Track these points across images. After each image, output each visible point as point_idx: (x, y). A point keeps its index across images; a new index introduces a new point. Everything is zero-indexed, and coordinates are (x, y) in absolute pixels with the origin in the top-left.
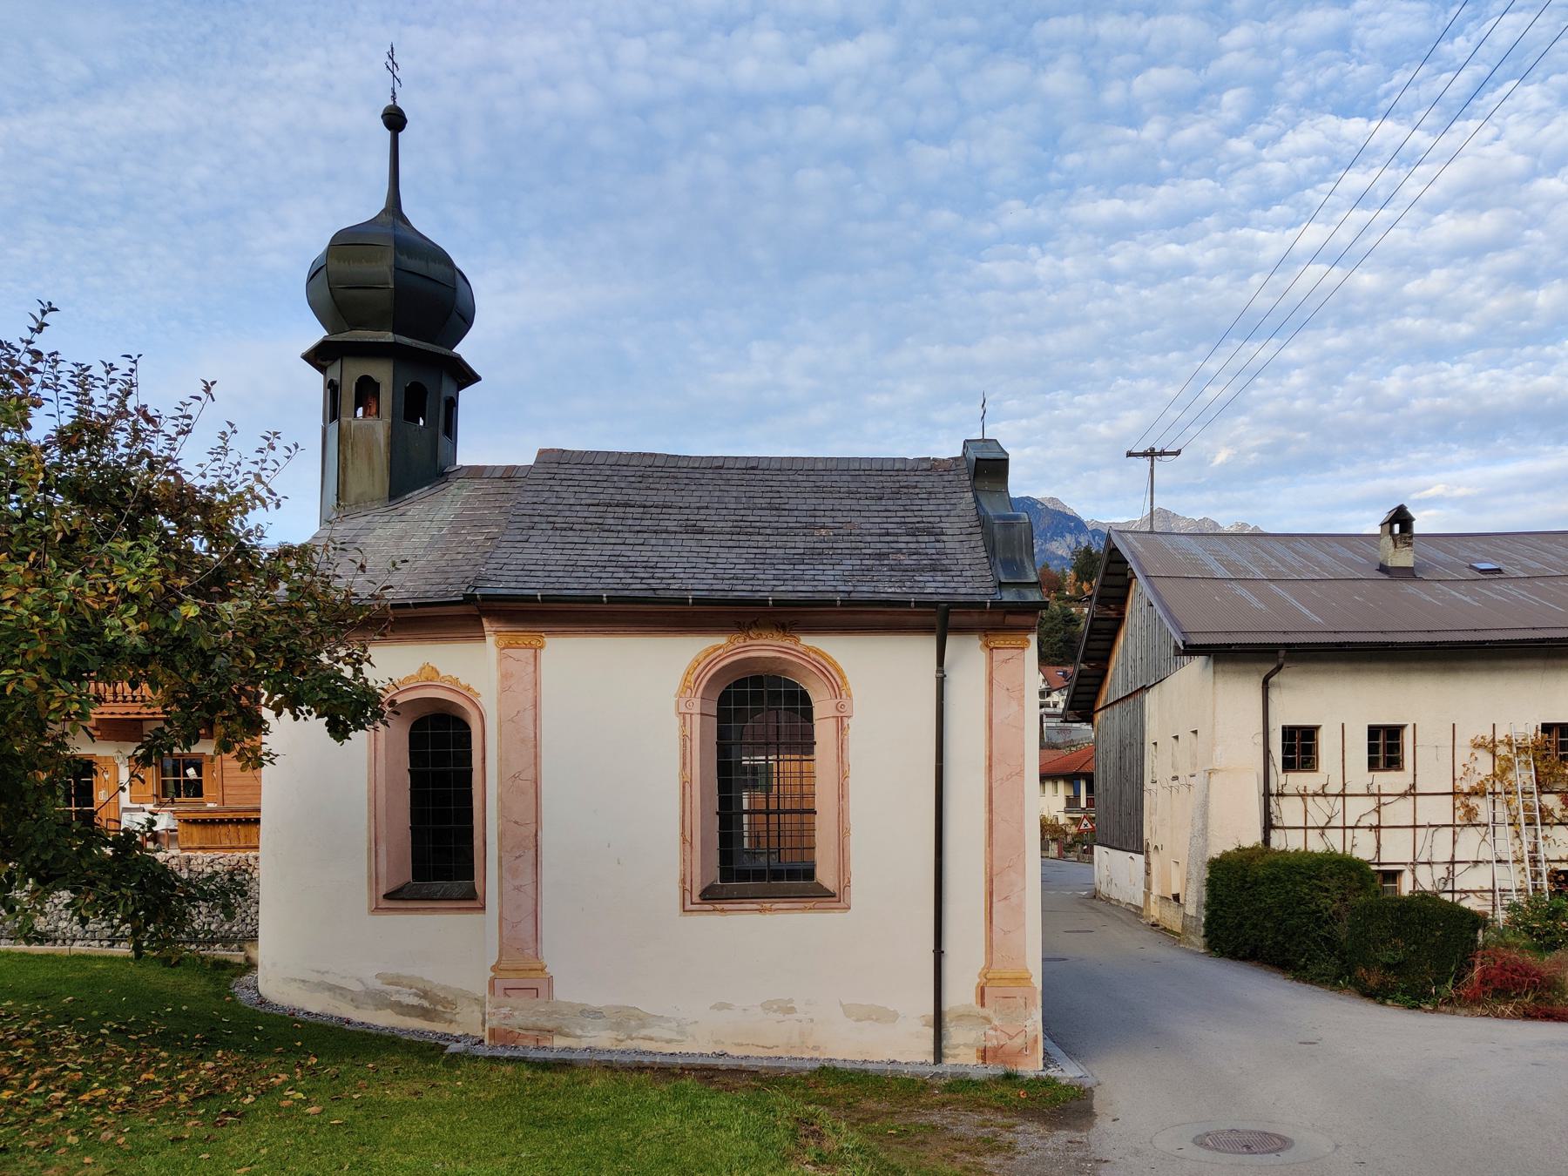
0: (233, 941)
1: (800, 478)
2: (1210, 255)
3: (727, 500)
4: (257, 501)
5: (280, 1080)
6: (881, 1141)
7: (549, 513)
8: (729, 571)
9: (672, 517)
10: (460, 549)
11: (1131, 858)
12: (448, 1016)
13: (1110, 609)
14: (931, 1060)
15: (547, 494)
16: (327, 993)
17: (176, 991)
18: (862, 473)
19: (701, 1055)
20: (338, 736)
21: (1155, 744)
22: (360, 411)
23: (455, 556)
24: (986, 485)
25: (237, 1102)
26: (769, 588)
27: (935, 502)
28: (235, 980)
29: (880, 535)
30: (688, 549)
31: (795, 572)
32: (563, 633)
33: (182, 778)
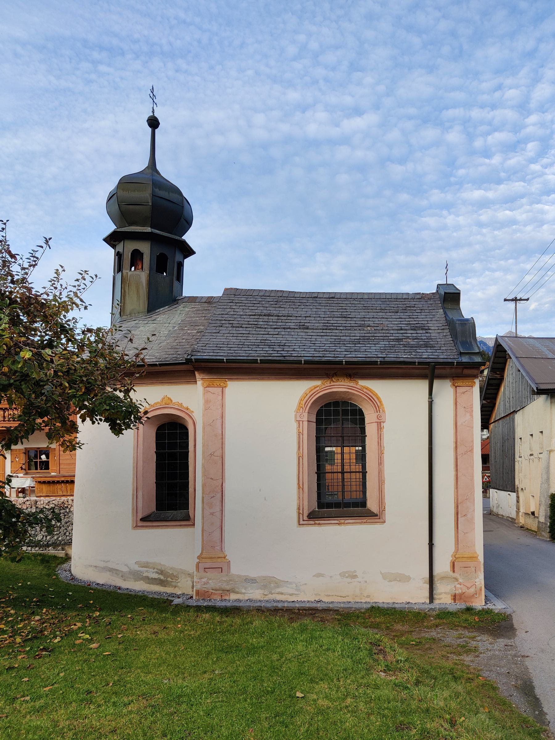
0: (59, 545)
1: (356, 302)
2: (524, 216)
3: (320, 313)
4: (74, 305)
5: (77, 627)
6: (408, 648)
7: (230, 319)
8: (322, 347)
9: (292, 321)
10: (184, 337)
11: (509, 494)
12: (174, 584)
13: (497, 374)
14: (428, 601)
15: (229, 310)
16: (108, 573)
17: (25, 574)
18: (387, 300)
19: (308, 602)
20: (116, 432)
21: (521, 438)
22: (133, 269)
23: (181, 341)
24: (449, 306)
25: (50, 642)
26: (343, 356)
27: (424, 314)
28: (59, 566)
29: (398, 330)
30: (301, 337)
31: (356, 348)
32: (237, 379)
33: (38, 460)
